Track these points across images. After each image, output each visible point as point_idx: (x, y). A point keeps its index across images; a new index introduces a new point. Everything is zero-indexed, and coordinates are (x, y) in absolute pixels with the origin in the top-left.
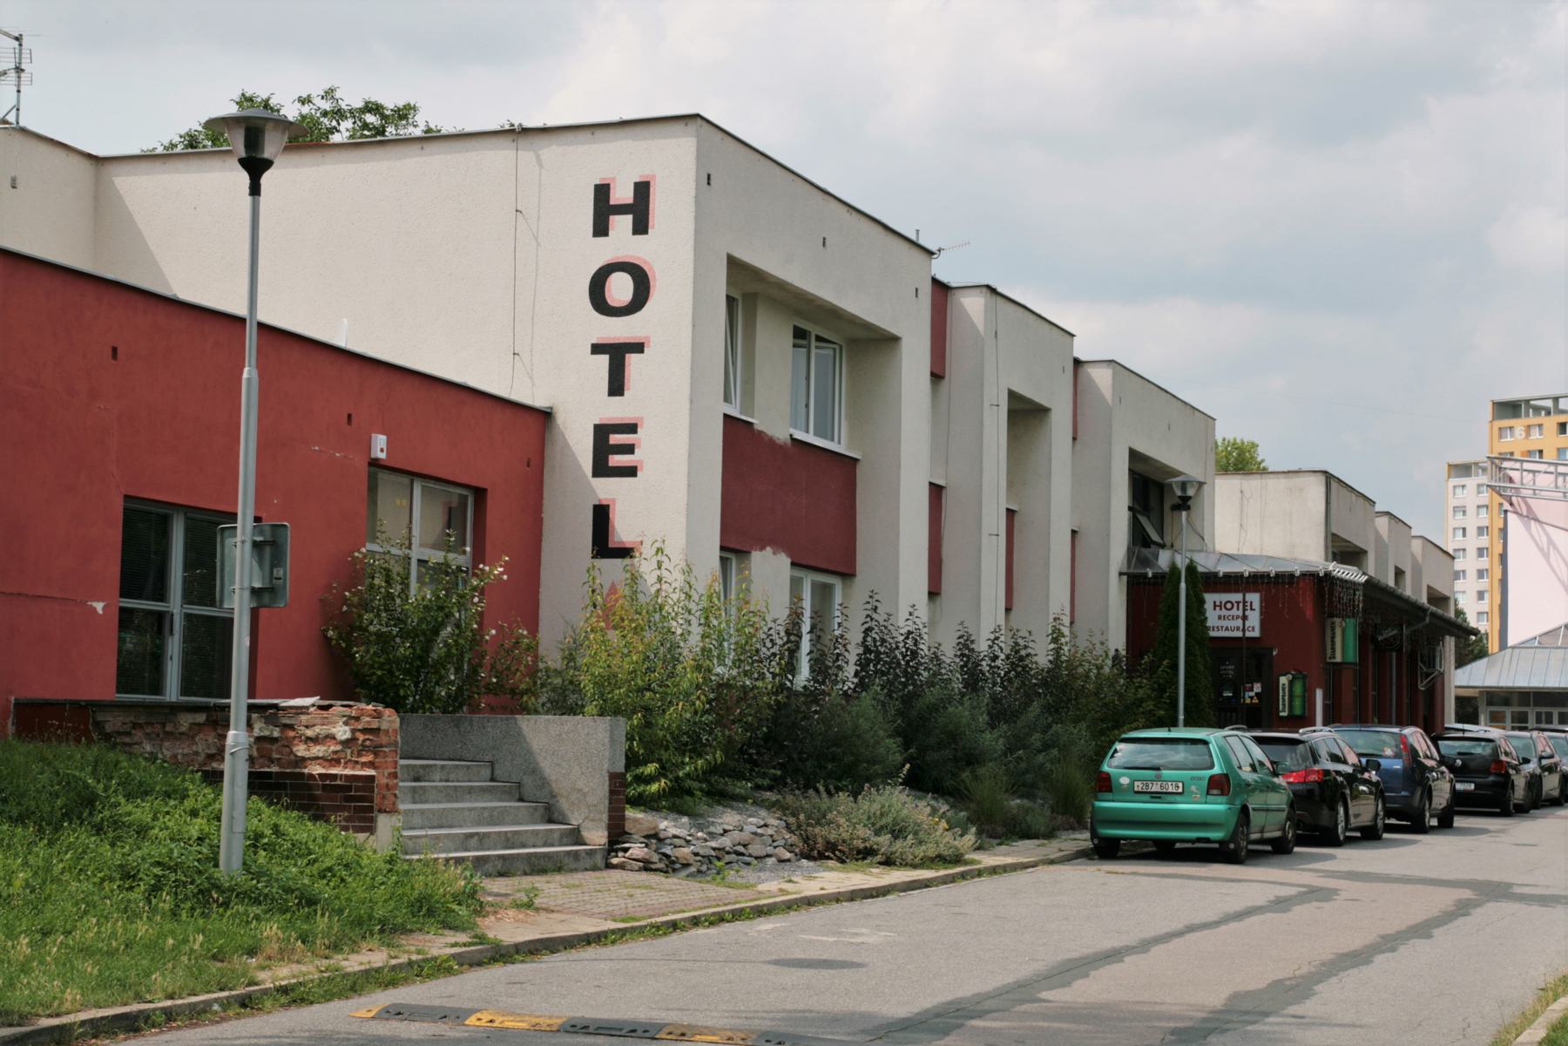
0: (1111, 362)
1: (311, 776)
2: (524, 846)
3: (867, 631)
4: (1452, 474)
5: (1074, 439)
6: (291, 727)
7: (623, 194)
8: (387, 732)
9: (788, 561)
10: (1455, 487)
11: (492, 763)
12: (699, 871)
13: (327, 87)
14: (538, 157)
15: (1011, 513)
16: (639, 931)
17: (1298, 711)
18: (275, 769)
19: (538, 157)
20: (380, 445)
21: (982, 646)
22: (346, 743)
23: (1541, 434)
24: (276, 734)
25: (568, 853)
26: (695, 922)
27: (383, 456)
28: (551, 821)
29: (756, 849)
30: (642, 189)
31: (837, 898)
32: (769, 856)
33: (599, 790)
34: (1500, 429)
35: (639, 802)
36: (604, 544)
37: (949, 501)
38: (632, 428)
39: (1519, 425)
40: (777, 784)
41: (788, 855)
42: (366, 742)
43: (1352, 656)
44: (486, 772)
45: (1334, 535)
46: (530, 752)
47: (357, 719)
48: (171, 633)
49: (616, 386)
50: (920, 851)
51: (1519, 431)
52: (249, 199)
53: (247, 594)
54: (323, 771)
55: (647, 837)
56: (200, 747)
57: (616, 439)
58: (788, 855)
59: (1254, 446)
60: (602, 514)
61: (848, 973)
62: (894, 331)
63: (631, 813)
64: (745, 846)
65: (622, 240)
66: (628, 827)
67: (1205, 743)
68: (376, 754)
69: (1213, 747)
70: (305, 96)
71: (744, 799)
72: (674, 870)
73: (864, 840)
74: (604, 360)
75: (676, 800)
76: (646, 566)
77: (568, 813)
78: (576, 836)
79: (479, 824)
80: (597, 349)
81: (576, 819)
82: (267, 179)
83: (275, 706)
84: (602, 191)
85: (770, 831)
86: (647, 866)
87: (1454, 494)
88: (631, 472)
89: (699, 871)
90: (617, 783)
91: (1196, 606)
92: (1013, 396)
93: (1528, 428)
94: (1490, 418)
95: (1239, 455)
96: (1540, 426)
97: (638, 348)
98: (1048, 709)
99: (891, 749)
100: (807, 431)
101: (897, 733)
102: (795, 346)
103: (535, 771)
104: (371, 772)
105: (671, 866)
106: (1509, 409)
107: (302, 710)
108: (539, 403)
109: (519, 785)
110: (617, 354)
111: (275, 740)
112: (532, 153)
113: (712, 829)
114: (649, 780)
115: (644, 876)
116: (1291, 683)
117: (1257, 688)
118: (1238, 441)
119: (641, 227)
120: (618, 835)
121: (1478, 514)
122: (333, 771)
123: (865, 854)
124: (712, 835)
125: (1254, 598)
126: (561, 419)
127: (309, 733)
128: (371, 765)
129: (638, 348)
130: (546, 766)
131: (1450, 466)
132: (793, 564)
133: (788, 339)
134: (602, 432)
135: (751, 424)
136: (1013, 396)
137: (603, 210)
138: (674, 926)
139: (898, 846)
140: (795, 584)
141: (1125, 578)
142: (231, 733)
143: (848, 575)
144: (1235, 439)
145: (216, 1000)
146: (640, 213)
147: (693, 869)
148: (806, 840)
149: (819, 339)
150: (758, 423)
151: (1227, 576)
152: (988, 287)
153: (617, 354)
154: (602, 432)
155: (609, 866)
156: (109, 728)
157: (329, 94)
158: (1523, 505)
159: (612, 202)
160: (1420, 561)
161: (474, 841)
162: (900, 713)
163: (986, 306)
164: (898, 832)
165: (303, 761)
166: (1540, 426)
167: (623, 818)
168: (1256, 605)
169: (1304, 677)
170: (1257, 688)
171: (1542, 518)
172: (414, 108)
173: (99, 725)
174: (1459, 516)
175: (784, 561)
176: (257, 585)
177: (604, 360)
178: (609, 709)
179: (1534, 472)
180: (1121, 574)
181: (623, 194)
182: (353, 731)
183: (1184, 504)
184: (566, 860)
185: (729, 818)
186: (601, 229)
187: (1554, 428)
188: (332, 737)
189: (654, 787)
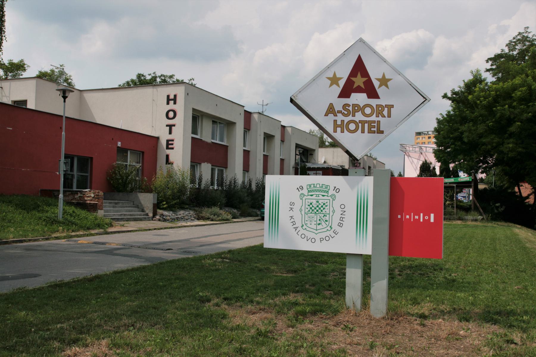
0: (291, 127)
1: (87, 203)
2: (135, 216)
6: (84, 194)
7: (172, 97)
8: (100, 195)
9: (211, 165)
11: (133, 202)
12: (171, 221)
13: (154, 72)
14: (157, 90)
18: (82, 202)
19: (157, 90)
20: (119, 144)
22: (93, 197)
24: (82, 196)
25: (143, 218)
27: (120, 146)
28: (143, 212)
29: (186, 218)
30: (175, 96)
32: (189, 219)
33: (151, 207)
36: (168, 161)
38: (173, 140)
39: (420, 137)
41: (193, 219)
42: (97, 197)
44: (132, 203)
46: (140, 200)
47: (95, 193)
48: (74, 178)
49: (170, 133)
50: (218, 219)
51: (421, 138)
52: (63, 103)
53: (63, 171)
54: (89, 202)
55: (161, 215)
56: (70, 198)
57: (170, 142)
58: (193, 219)
60: (167, 156)
61: (167, 236)
62: (234, 121)
64: (184, 217)
65: (172, 106)
66: (157, 213)
68: (98, 199)
70: (149, 73)
72: (166, 221)
73: (208, 216)
74: (168, 128)
75: (170, 208)
76: (175, 165)
77: (146, 210)
78: (147, 215)
79: (126, 212)
80: (167, 126)
81: (147, 212)
82: (67, 100)
83: (82, 191)
84: (168, 96)
85: (190, 214)
86: (159, 220)
88: (173, 148)
89: (171, 221)
92: (265, 133)
93: (422, 138)
96: (425, 137)
97: (174, 125)
100: (217, 140)
102: (212, 124)
103: (140, 203)
104: (97, 202)
105: (165, 220)
106: (419, 134)
107: (86, 192)
108: (156, 135)
109: (138, 206)
110: (170, 126)
111: (82, 197)
112: (156, 89)
113: (177, 214)
115: (159, 222)
119: (175, 103)
120: (155, 214)
122: (91, 202)
123: (208, 219)
124: (177, 215)
126: (161, 139)
127: (87, 195)
128: (97, 201)
129: (174, 125)
130: (142, 202)
132: (212, 166)
133: (211, 123)
135: (202, 139)
136: (265, 133)
137: (168, 100)
138: (150, 230)
139: (214, 218)
140: (213, 170)
141: (294, 168)
142: (60, 195)
143: (226, 167)
145: (41, 238)
146: (175, 100)
147: (170, 221)
149: (219, 123)
150: (203, 139)
151: (313, 168)
152: (258, 113)
153: (170, 126)
154: (168, 141)
155: (153, 220)
156: (55, 194)
157: (154, 73)
159: (170, 98)
160: (376, 164)
161: (123, 215)
163: (258, 117)
165: (86, 200)
166: (425, 137)
167: (157, 211)
172: (174, 75)
173: (54, 194)
176: (65, 170)
177: (168, 128)
179: (415, 148)
180: (293, 167)
181: (172, 97)
182: (94, 195)
183: (312, 154)
184: (143, 219)
185: (182, 212)
186: (168, 103)
188: (91, 196)
189: (165, 206)
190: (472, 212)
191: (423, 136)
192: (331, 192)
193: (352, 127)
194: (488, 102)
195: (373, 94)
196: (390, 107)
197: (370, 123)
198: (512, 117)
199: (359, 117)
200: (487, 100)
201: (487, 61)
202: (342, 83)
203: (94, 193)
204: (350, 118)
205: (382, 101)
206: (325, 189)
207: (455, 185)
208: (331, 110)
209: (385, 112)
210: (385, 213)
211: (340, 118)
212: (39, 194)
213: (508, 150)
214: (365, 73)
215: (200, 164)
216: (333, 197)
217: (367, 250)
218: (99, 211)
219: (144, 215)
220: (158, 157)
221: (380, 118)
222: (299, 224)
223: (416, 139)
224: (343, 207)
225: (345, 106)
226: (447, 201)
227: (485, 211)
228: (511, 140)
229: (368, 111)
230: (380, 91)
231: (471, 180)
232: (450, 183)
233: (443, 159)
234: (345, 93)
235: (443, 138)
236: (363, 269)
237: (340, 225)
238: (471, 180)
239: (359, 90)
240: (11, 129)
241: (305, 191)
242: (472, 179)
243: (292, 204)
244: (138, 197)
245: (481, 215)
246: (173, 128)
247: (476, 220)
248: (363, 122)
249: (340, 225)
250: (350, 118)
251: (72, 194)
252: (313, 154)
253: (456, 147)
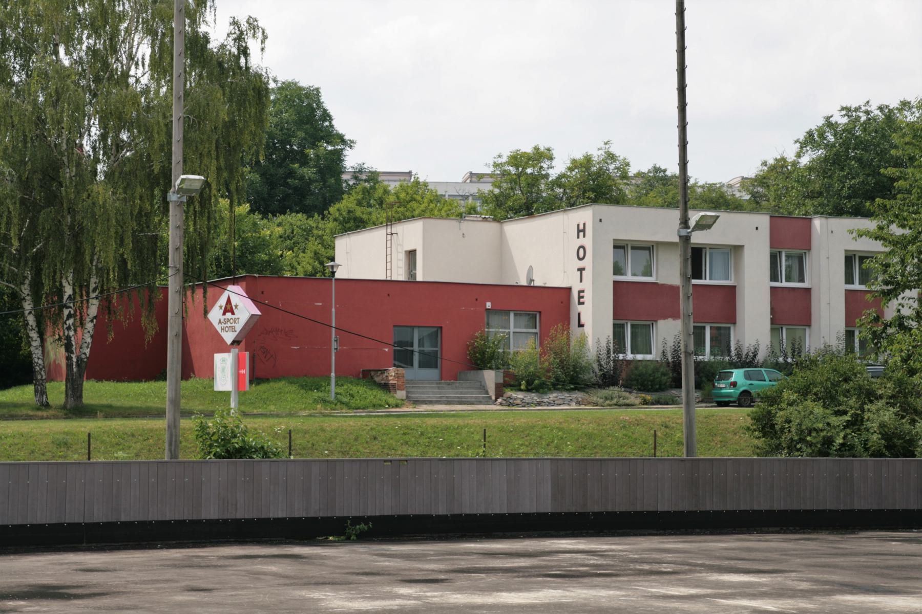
21: (744, 353)
27: (490, 307)
62: (742, 244)
67: (770, 381)
74: (579, 272)
110: (581, 270)
135: (657, 283)
144: (323, 103)
153: (581, 270)
154: (580, 292)
177: (579, 272)
195: (233, 313)
196: (238, 319)
197: (232, 327)
202: (223, 308)
208: (220, 322)
211: (223, 325)
212: (361, 375)
215: (656, 321)
218: (398, 392)
220: (571, 316)
229: (231, 321)
230: (235, 311)
234: (224, 314)
236: (237, 402)
239: (228, 311)
240: (320, 304)
246: (583, 272)
250: (226, 325)
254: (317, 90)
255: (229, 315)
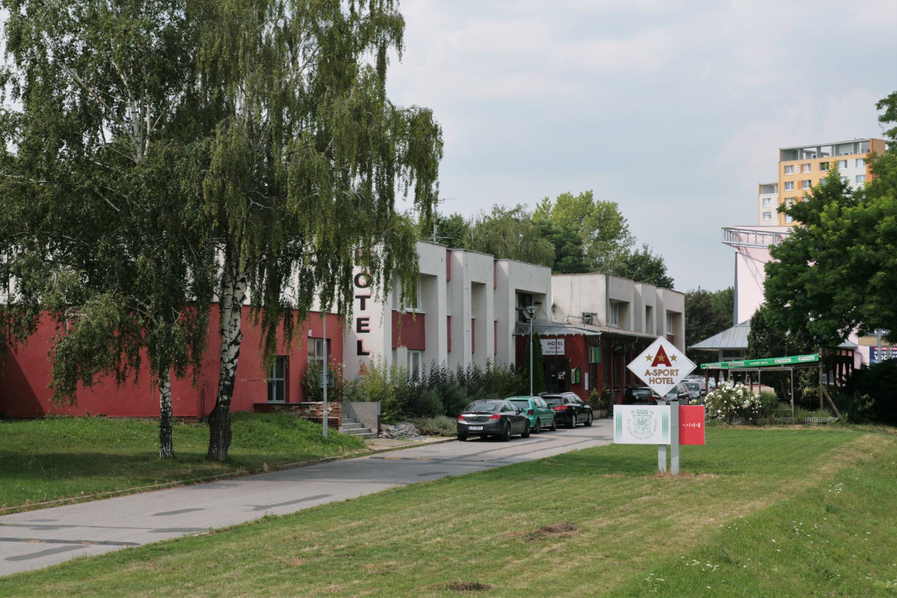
3: (432, 371)
4: (763, 191)
5: (495, 288)
10: (764, 200)
15: (473, 320)
16: (396, 449)
17: (578, 382)
21: (465, 372)
23: (810, 170)
26: (406, 447)
29: (409, 433)
31: (433, 443)
34: (785, 167)
35: (384, 422)
36: (360, 352)
37: (452, 320)
38: (367, 319)
39: (796, 164)
40: (412, 416)
43: (598, 360)
45: (611, 300)
50: (450, 433)
51: (797, 168)
57: (363, 322)
59: (615, 205)
60: (360, 343)
63: (382, 425)
67: (527, 401)
69: (529, 402)
71: (404, 420)
75: (390, 422)
78: (370, 431)
86: (387, 437)
87: (764, 204)
88: (368, 331)
90: (380, 417)
91: (538, 347)
94: (779, 160)
95: (606, 210)
98: (485, 389)
99: (440, 405)
101: (442, 400)
105: (393, 437)
106: (790, 154)
114: (385, 416)
116: (576, 371)
117: (564, 373)
118: (606, 202)
120: (380, 431)
121: (857, 165)
123: (436, 434)
125: (562, 341)
131: (760, 186)
134: (359, 320)
139: (445, 431)
140: (409, 354)
143: (423, 349)
144: (604, 201)
148: (421, 430)
158: (745, 251)
162: (443, 395)
164: (445, 428)
166: (809, 165)
168: (563, 343)
169: (580, 370)
170: (564, 373)
171: (752, 257)
174: (767, 218)
175: (406, 349)
178: (373, 400)
179: (748, 233)
187: (818, 166)
189: (386, 418)
190: (821, 412)
191: (805, 160)
192: (649, 413)
193: (659, 381)
194: (840, 237)
196: (677, 371)
197: (667, 379)
198: (873, 262)
199: (662, 376)
200: (838, 233)
201: (879, 106)
202: (653, 359)
203: (332, 407)
204: (658, 376)
205: (674, 367)
206: (646, 412)
207: (791, 369)
208: (648, 373)
209: (675, 373)
210: (677, 424)
211: (652, 377)
213: (868, 313)
214: (664, 354)
216: (650, 416)
217: (668, 441)
219: (364, 431)
221: (672, 376)
222: (633, 431)
223: (782, 168)
224: (655, 421)
225: (655, 371)
226: (805, 386)
227: (842, 407)
228: (875, 298)
229: (666, 373)
230: (672, 362)
231: (817, 360)
232: (786, 365)
233: (776, 322)
234: (655, 364)
235: (776, 287)
237: (654, 430)
238: (817, 360)
239: (661, 362)
241: (636, 413)
242: (819, 358)
243: (629, 420)
244: (351, 407)
245: (835, 415)
247: (824, 423)
248: (664, 379)
249: (654, 430)
250: (658, 376)
251: (300, 408)
252: (541, 303)
253: (796, 304)
254: (426, 115)
255: (661, 367)
